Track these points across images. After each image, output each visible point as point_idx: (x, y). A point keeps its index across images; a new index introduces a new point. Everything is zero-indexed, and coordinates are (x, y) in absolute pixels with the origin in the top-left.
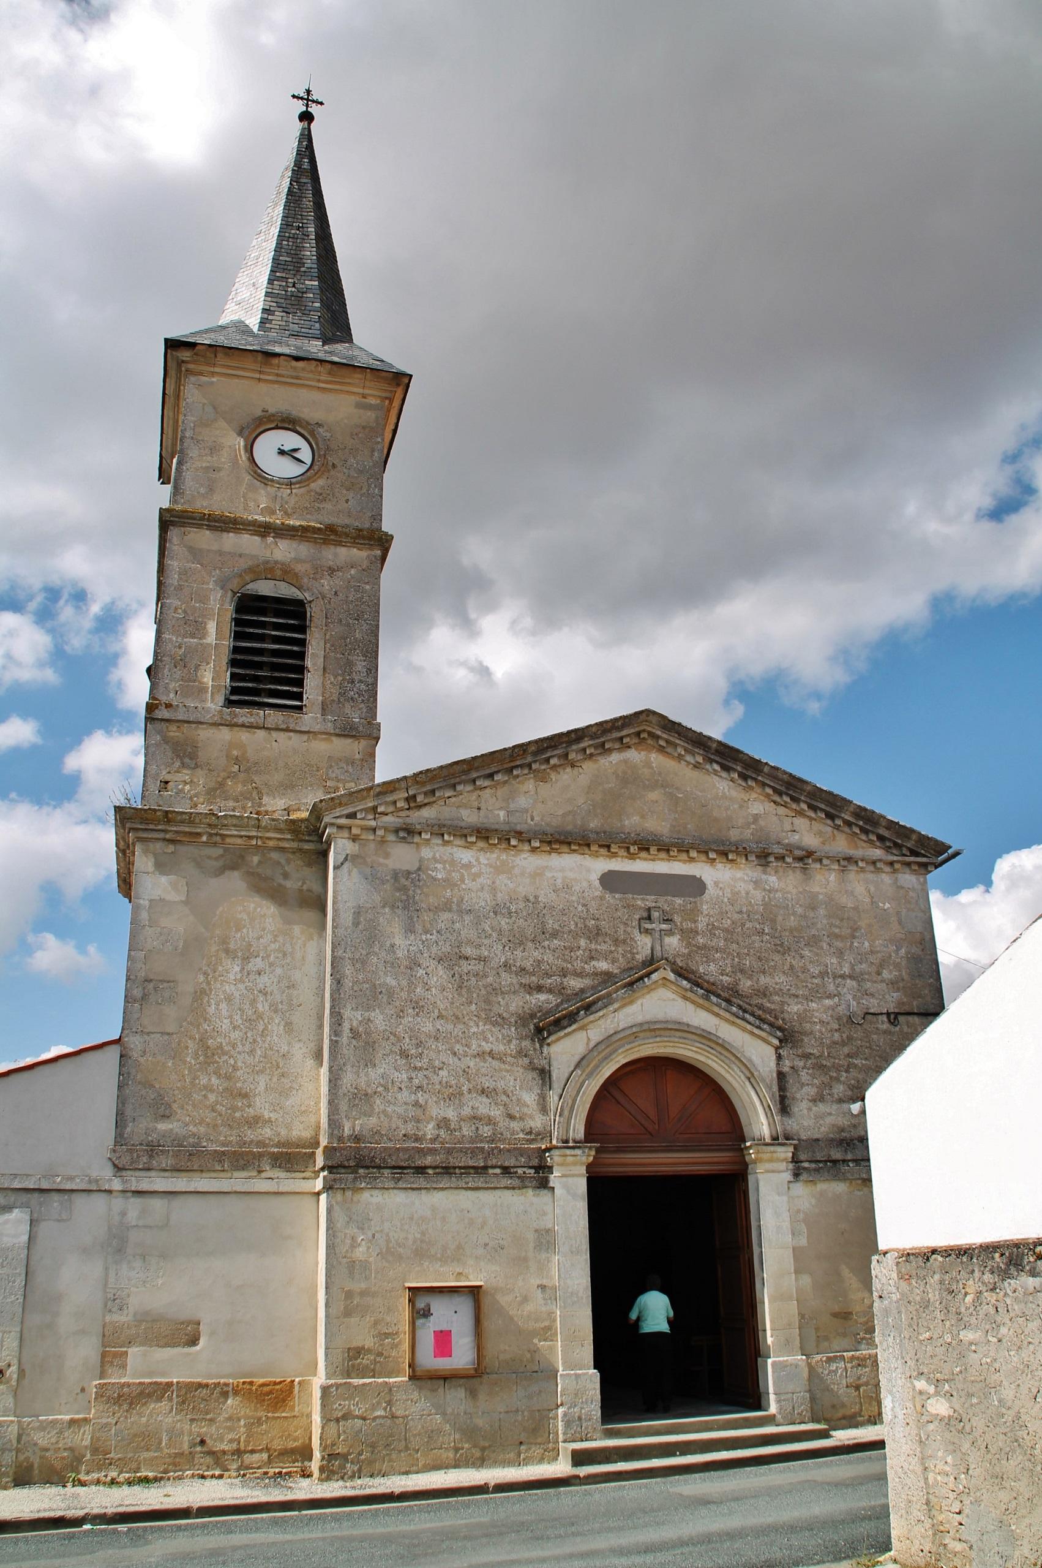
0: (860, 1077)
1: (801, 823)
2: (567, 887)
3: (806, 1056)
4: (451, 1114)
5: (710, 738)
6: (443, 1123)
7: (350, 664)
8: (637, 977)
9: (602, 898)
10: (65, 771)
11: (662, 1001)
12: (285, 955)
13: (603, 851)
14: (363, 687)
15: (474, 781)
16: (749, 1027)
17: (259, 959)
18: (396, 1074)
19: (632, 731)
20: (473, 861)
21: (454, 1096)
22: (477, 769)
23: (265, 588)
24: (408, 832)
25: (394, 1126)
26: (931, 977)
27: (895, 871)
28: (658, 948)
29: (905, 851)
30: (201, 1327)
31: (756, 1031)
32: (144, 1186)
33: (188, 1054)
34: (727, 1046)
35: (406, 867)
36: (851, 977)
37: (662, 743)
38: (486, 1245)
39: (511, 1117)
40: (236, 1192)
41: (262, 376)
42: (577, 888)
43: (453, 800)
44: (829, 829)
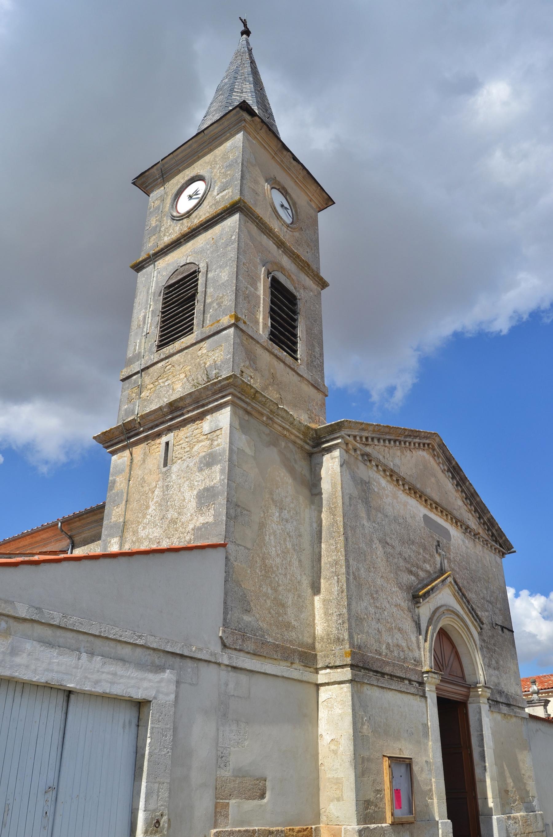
10: (505, 331)
17: (286, 511)
30: (267, 783)
32: (240, 664)
40: (283, 677)
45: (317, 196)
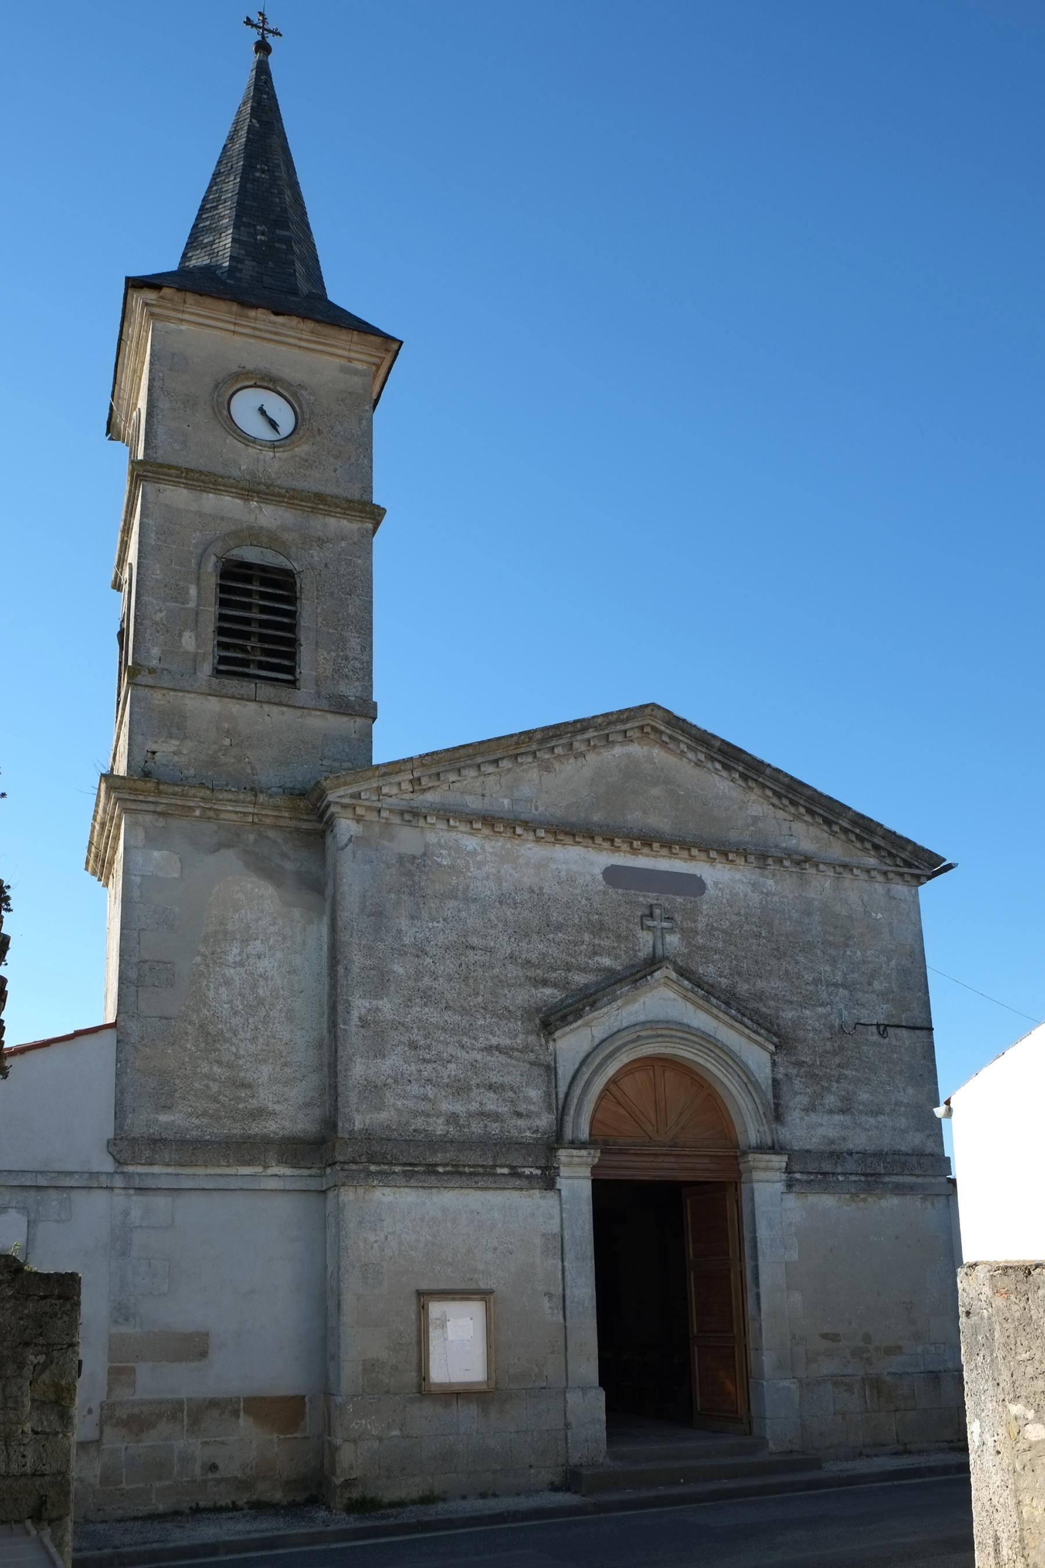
0: (850, 1088)
1: (798, 827)
2: (571, 880)
3: (800, 1064)
4: (459, 1108)
5: (714, 736)
6: (452, 1118)
7: (343, 640)
8: (641, 972)
9: (605, 893)
11: (661, 1001)
12: (285, 938)
13: (606, 845)
14: (358, 665)
15: (479, 766)
16: (746, 1031)
17: (258, 942)
18: (405, 1066)
19: (636, 724)
20: (478, 848)
21: (460, 1089)
22: (482, 754)
23: (251, 555)
24: (413, 815)
25: (404, 1120)
26: (919, 990)
27: (888, 880)
28: (659, 946)
29: (899, 862)
31: (753, 1035)
33: (187, 1040)
34: (725, 1049)
35: (411, 851)
36: (844, 986)
37: (665, 738)
38: (495, 1249)
39: (519, 1115)
40: (241, 1189)
41: (238, 329)
42: (580, 881)
43: (457, 785)
44: (826, 835)
45: (359, 348)
